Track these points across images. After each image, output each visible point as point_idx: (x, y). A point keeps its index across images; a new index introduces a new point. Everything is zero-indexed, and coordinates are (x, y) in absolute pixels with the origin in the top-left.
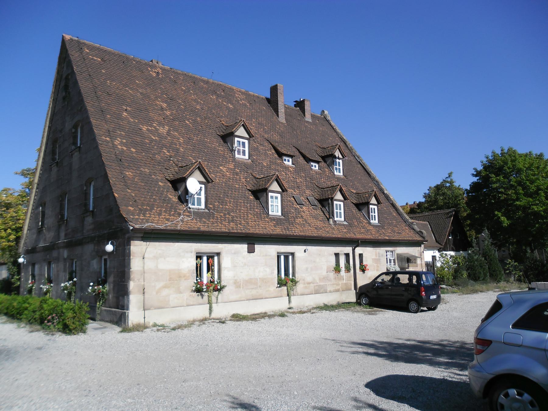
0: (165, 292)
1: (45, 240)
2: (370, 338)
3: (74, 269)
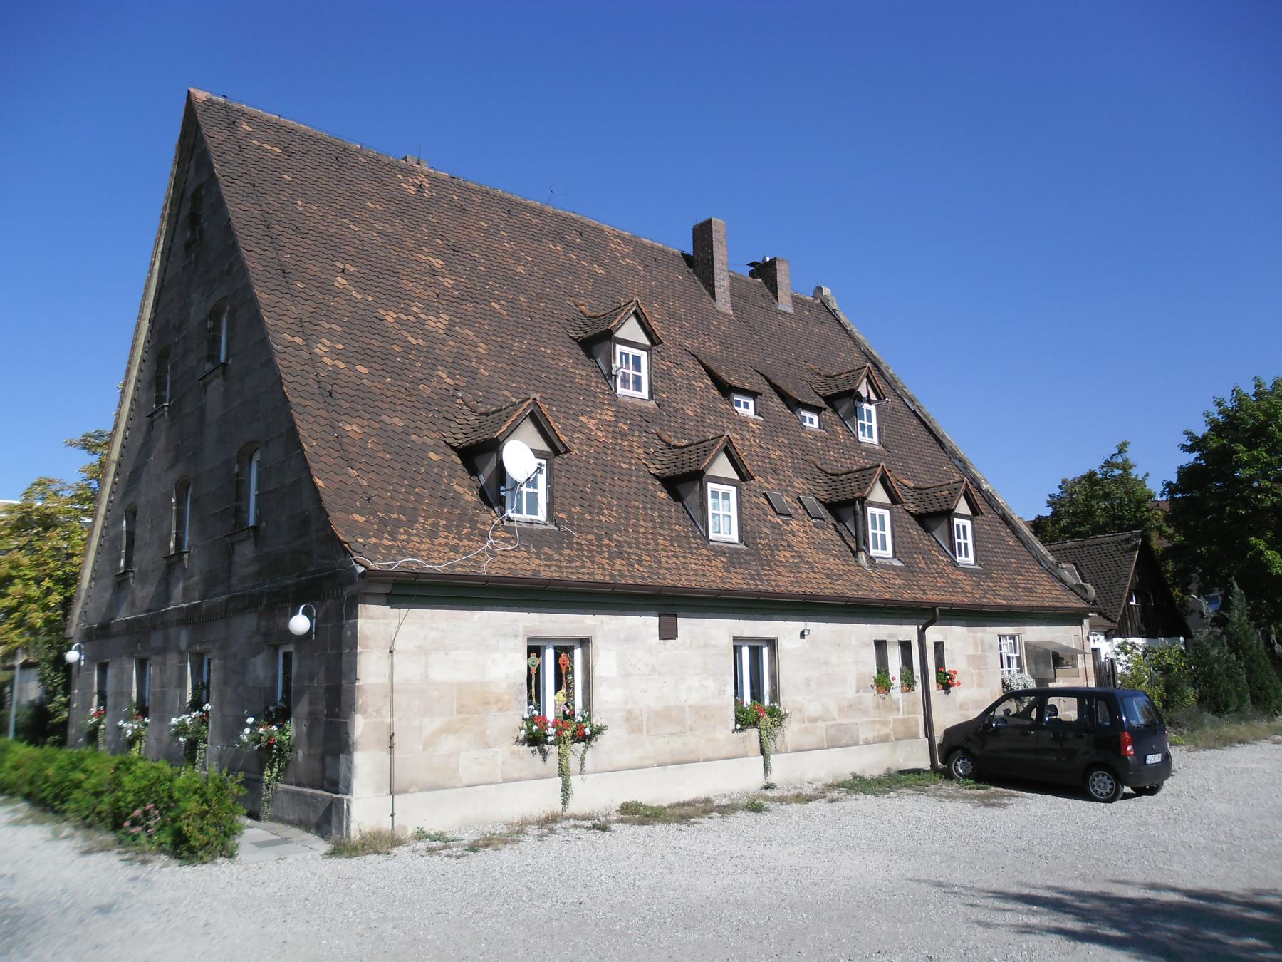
0: (448, 744)
1: (133, 604)
2: (1040, 880)
3: (205, 680)
